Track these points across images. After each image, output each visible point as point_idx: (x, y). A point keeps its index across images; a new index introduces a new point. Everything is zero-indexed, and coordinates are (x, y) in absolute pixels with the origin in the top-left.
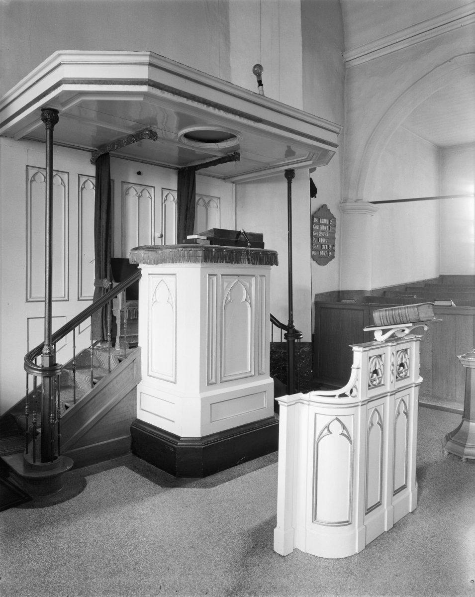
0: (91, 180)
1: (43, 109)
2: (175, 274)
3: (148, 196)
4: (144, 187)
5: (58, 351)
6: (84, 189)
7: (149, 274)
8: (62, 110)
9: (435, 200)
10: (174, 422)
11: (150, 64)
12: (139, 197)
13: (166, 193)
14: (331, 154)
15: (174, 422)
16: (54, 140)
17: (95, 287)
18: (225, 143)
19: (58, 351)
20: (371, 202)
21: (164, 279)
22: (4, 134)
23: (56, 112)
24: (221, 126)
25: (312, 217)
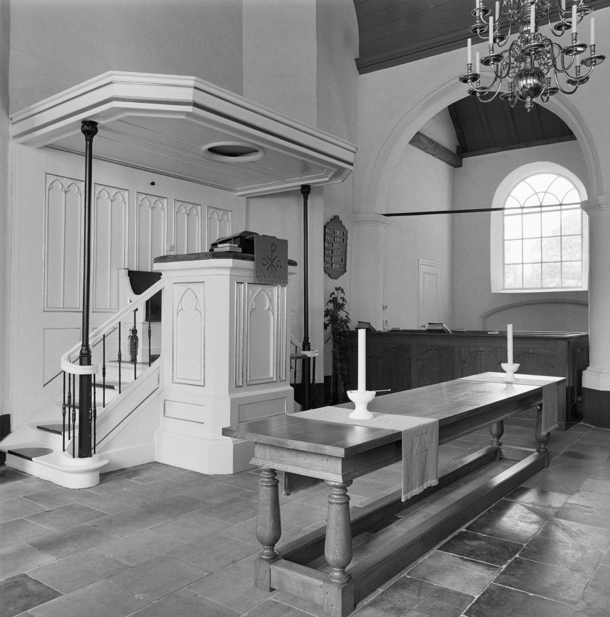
0: (121, 193)
1: (85, 122)
2: (204, 282)
3: (226, 219)
4: (56, 178)
5: (77, 360)
6: (99, 199)
7: (174, 283)
8: (101, 122)
9: (448, 214)
10: (203, 423)
11: (195, 80)
12: (66, 192)
13: (50, 179)
14: (347, 172)
15: (203, 423)
16: (93, 154)
17: (309, 341)
18: (251, 157)
19: (77, 360)
20: (384, 215)
21: (191, 287)
22: (27, 142)
23: (96, 123)
24: (33, 109)
25: (325, 227)
